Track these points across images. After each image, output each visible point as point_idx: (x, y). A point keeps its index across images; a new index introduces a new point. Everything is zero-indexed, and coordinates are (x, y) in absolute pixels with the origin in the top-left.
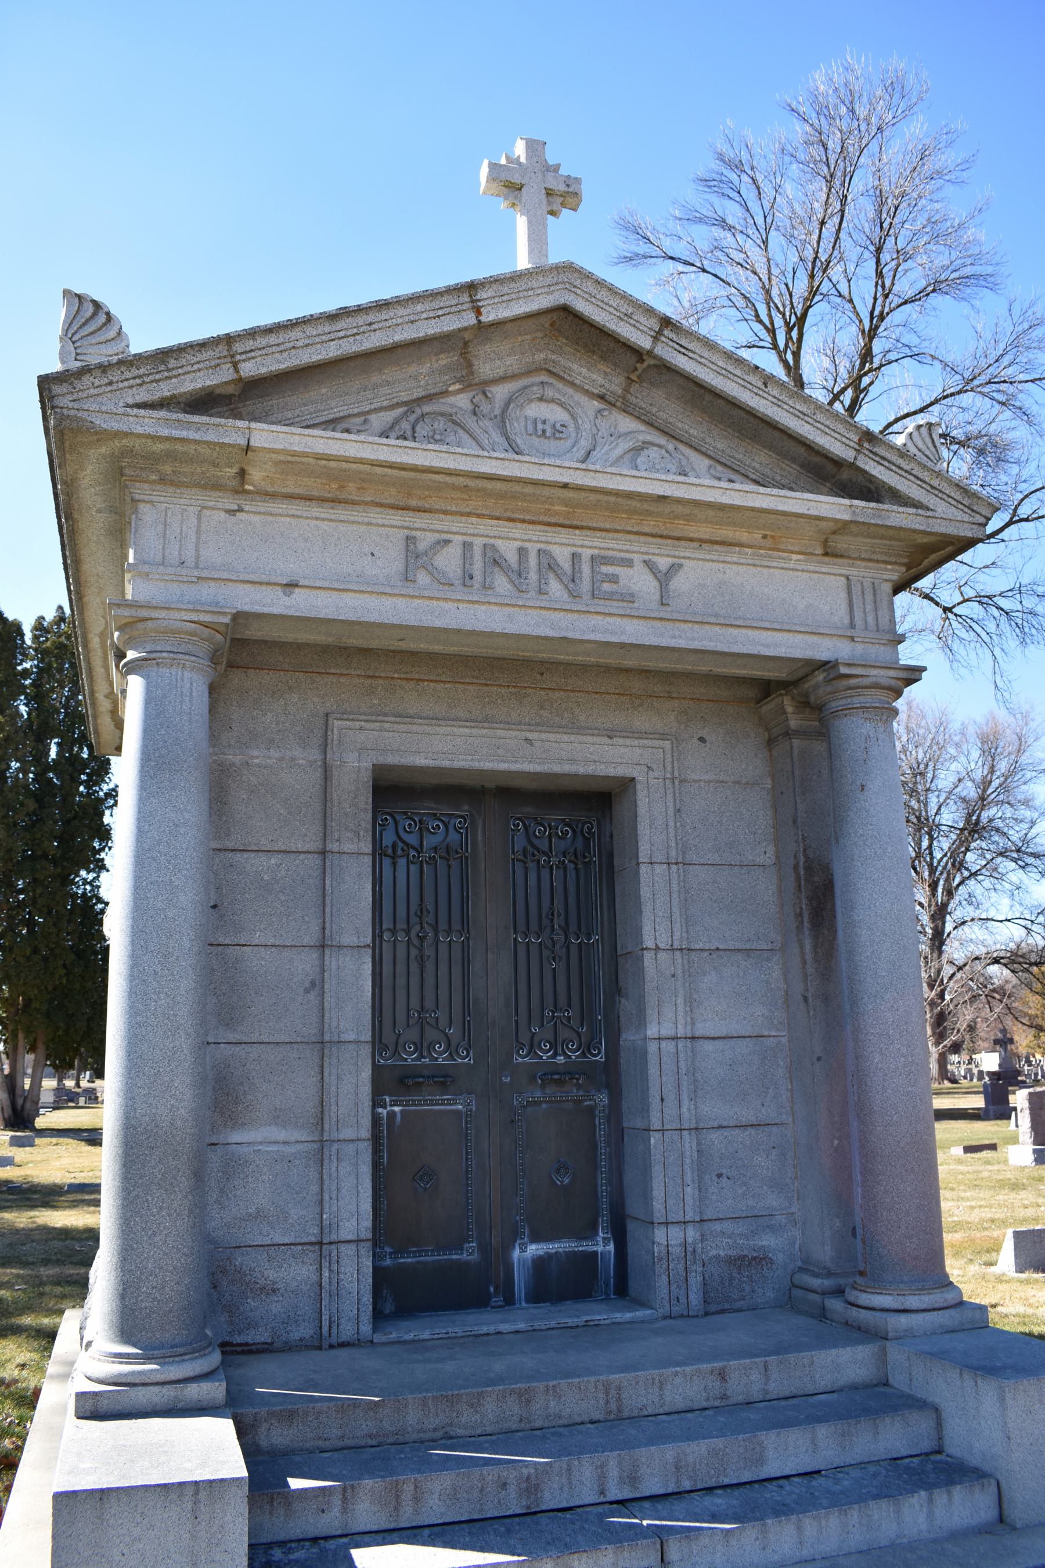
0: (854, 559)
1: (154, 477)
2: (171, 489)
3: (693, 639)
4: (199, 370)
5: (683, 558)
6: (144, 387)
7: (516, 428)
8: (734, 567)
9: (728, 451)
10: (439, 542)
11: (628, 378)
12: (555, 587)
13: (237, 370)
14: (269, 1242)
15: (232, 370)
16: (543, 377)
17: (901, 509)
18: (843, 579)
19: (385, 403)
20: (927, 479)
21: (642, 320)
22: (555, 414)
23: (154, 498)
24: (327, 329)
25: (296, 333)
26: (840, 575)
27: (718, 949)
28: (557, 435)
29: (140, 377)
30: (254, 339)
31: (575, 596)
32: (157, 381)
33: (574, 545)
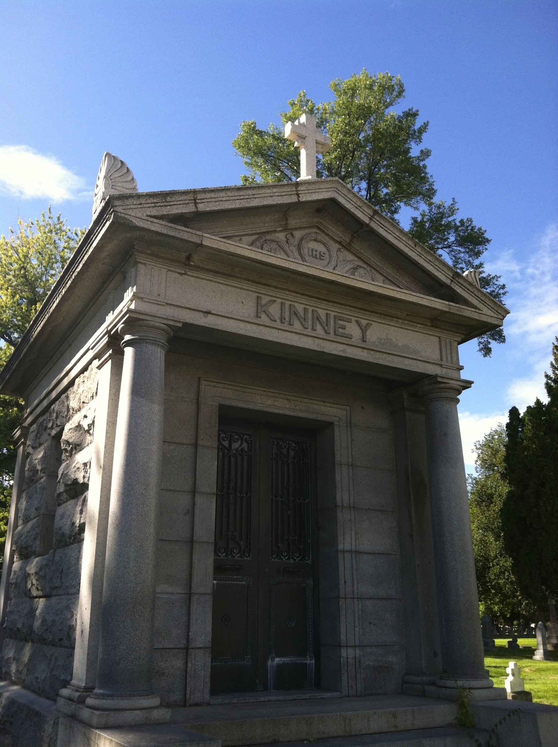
0: (443, 329)
1: (149, 252)
2: (156, 259)
3: (376, 358)
4: (180, 204)
5: (372, 321)
6: (156, 208)
7: (305, 252)
8: (393, 328)
9: (392, 274)
10: (271, 301)
11: (352, 235)
12: (319, 327)
13: (196, 207)
14: (162, 647)
15: (194, 207)
16: (315, 230)
17: (469, 309)
18: (438, 338)
19: (250, 232)
20: (480, 296)
21: (366, 210)
22: (321, 248)
23: (146, 262)
24: (236, 194)
25: (222, 194)
26: (437, 336)
27: (369, 509)
28: (322, 258)
29: (154, 203)
30: (205, 194)
31: (327, 333)
32: (161, 206)
33: (328, 310)
